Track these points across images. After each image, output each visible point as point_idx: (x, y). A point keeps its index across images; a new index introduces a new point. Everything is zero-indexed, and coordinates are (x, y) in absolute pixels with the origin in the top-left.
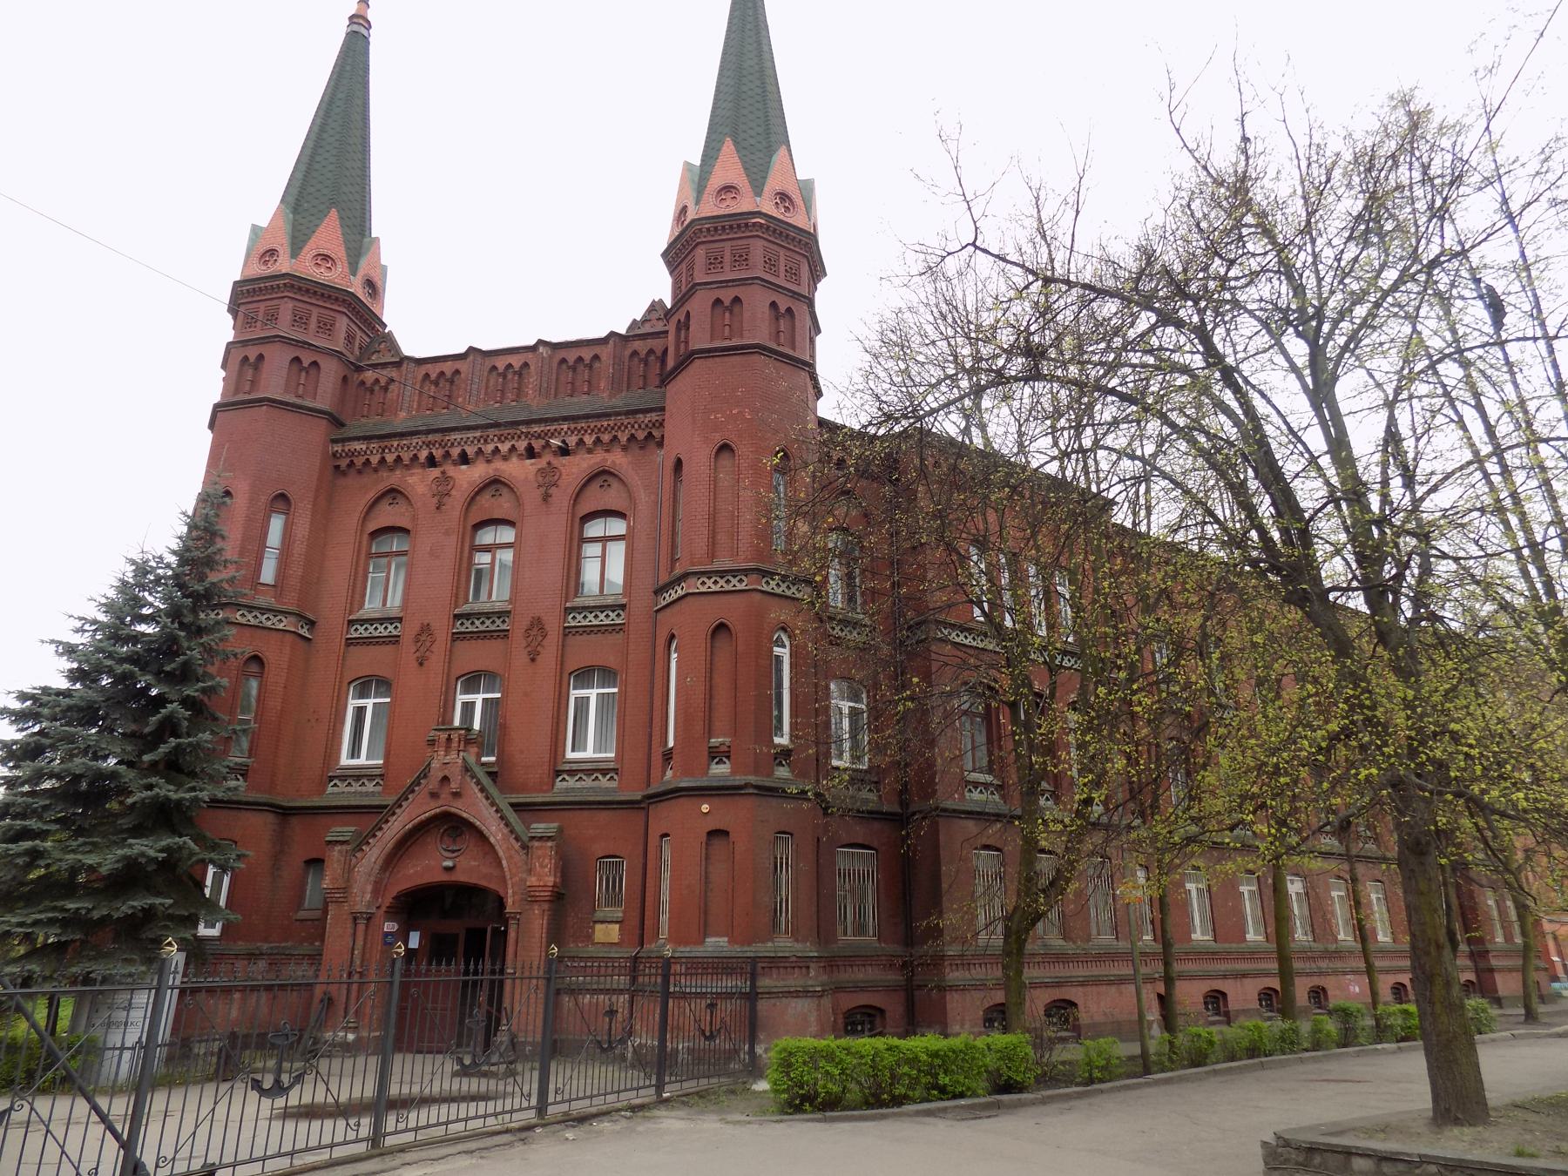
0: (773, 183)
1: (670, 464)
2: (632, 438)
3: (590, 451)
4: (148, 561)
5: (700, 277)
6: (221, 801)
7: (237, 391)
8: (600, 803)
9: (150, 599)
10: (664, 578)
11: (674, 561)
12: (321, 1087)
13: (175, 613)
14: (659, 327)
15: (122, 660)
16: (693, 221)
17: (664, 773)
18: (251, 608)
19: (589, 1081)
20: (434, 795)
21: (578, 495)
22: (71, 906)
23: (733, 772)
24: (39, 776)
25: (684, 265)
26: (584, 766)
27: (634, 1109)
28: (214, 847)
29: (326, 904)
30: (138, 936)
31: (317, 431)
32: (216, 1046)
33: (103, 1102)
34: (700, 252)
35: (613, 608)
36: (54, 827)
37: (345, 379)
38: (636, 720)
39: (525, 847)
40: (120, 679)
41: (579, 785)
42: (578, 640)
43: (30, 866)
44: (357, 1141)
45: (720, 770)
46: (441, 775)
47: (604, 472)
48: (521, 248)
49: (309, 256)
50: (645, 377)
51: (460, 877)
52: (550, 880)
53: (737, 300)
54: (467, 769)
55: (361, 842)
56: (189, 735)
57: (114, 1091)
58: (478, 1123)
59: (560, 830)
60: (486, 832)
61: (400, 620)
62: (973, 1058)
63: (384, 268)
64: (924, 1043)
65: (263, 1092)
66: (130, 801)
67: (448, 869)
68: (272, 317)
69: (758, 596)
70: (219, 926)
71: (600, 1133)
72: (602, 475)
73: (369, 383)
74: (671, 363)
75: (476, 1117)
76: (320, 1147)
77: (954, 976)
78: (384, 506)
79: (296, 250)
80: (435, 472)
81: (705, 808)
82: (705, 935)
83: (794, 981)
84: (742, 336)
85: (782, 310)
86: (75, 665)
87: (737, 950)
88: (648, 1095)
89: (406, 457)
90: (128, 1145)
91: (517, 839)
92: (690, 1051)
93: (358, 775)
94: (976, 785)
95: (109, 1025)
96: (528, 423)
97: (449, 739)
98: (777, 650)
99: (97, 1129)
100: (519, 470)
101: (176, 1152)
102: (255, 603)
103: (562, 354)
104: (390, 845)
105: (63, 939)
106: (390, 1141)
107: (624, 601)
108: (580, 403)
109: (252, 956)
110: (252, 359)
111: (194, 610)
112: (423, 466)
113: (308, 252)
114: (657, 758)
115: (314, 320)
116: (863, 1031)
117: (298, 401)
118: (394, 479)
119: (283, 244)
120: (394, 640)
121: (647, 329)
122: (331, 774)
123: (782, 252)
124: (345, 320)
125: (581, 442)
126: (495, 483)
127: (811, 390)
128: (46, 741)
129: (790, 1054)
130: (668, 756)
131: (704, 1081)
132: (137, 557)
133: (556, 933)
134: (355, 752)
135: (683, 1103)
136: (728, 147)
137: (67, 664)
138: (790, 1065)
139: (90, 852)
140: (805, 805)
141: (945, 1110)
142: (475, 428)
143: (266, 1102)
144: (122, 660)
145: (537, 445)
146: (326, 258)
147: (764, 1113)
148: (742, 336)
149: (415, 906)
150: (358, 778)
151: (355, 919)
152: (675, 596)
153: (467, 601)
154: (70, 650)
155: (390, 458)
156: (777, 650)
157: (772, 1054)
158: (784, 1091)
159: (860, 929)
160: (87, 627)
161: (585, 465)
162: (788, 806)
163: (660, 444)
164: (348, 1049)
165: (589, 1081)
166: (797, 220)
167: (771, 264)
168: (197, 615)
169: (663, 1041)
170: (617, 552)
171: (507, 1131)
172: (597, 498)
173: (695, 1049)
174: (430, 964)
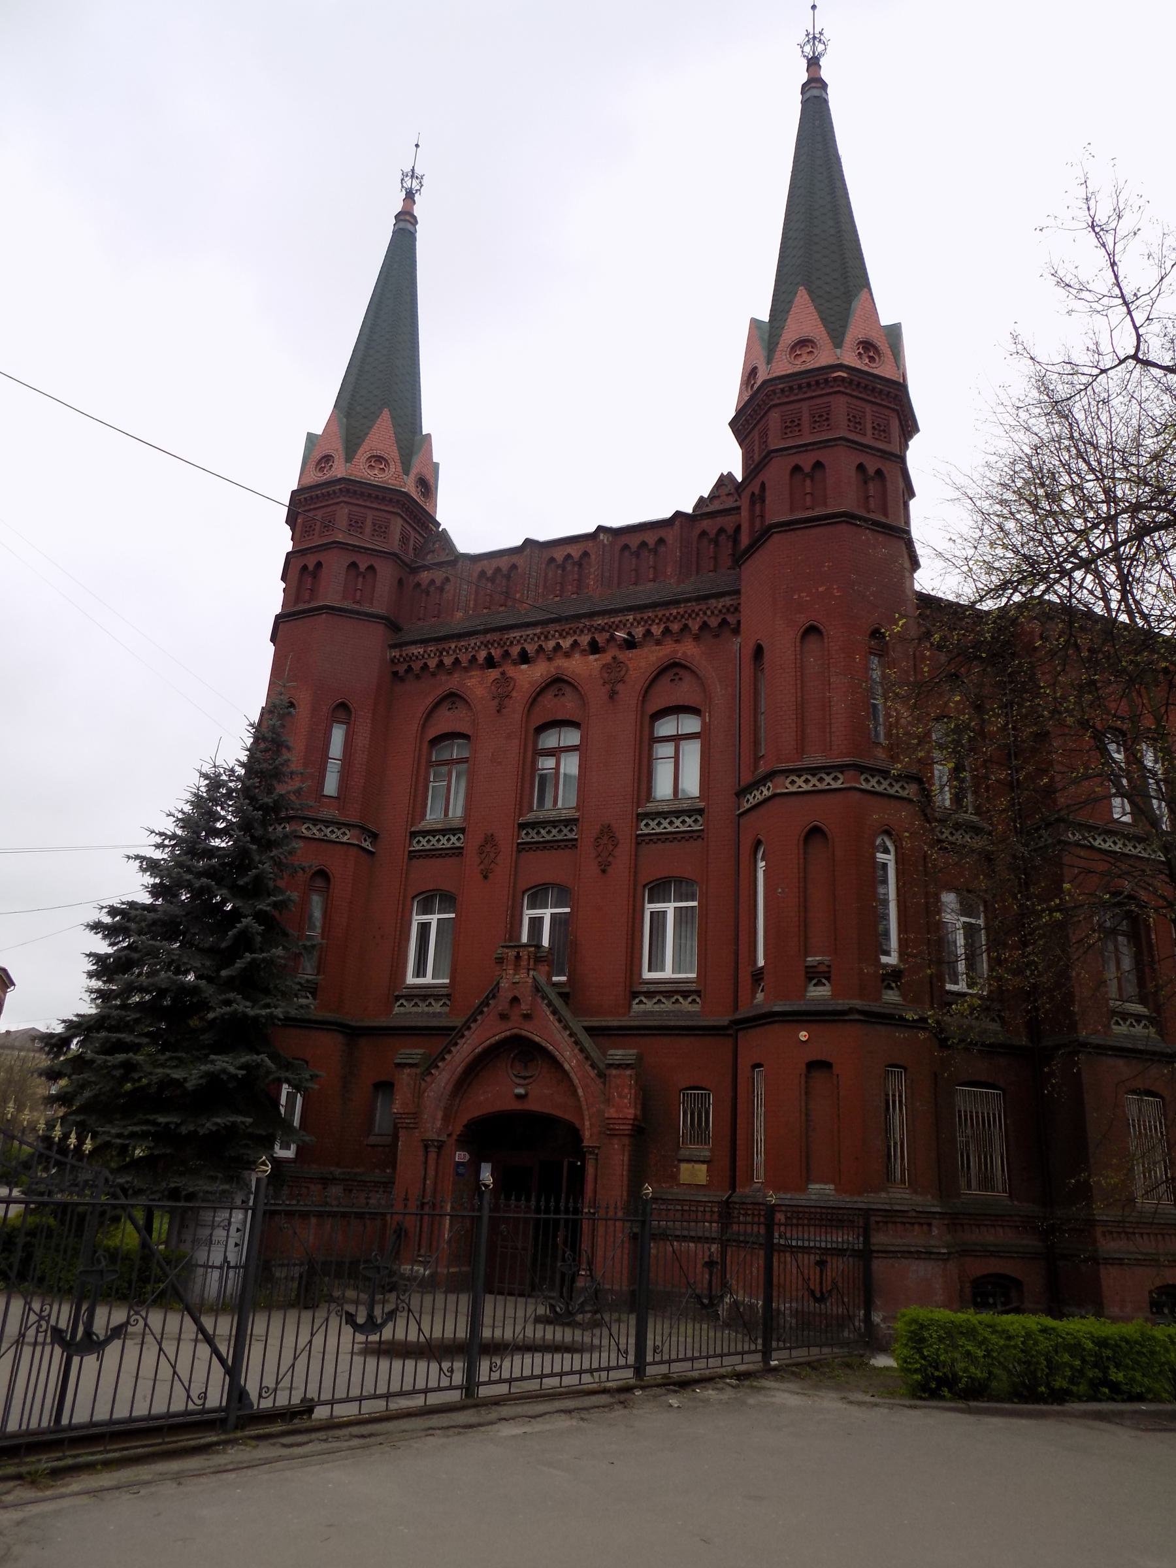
0: (855, 332)
1: (749, 651)
2: (704, 626)
4: (220, 775)
5: (775, 443)
6: (295, 1019)
7: (298, 599)
9: (223, 813)
10: (747, 778)
11: (757, 759)
12: (413, 1327)
13: (246, 825)
14: (730, 503)
15: (199, 875)
16: (765, 382)
17: (754, 997)
18: (315, 821)
19: (682, 1339)
20: (503, 1017)
21: (646, 691)
22: (162, 1120)
23: (834, 995)
24: (129, 989)
25: (756, 433)
26: (662, 988)
27: (740, 1376)
28: (288, 1066)
29: (396, 1128)
30: (225, 1157)
31: (373, 639)
32: (296, 1272)
33: (208, 1322)
34: (775, 415)
35: (689, 813)
36: (145, 1040)
37: (400, 581)
38: (719, 935)
39: (601, 1075)
40: (196, 894)
41: (657, 1008)
42: (645, 851)
43: (125, 1078)
44: (451, 1388)
45: (819, 993)
46: (510, 995)
47: (676, 665)
48: (585, 425)
49: (363, 459)
50: (715, 558)
51: (533, 1106)
52: (630, 1112)
53: (818, 465)
54: (537, 989)
55: (431, 1064)
56: (262, 951)
57: (218, 1309)
58: (554, 1382)
59: (640, 1057)
60: (559, 1057)
61: (463, 830)
62: (1153, 1353)
63: (437, 465)
64: (1080, 1327)
65: (357, 1328)
66: (211, 1016)
67: (519, 1097)
68: (328, 525)
69: (858, 795)
70: (293, 1147)
71: (706, 1401)
72: (673, 668)
73: (425, 583)
74: (745, 541)
75: (572, 1373)
76: (414, 1392)
77: (1109, 1246)
78: (444, 712)
79: (350, 454)
80: (494, 674)
81: (803, 1036)
82: (808, 1180)
83: (915, 1239)
84: (825, 504)
86: (158, 881)
87: (848, 1200)
88: (752, 1362)
89: (464, 659)
90: (233, 1371)
91: (593, 1066)
92: (796, 1314)
93: (424, 994)
94: (1125, 1016)
95: (195, 1241)
96: (592, 615)
97: (518, 957)
98: (881, 857)
99: (204, 1350)
100: (582, 666)
101: (277, 1383)
102: (320, 816)
103: (624, 540)
104: (460, 1069)
105: (156, 1152)
106: (483, 1391)
107: (702, 805)
108: (646, 592)
109: (326, 1181)
110: (311, 568)
111: (264, 823)
112: (482, 667)
114: (745, 978)
115: (369, 522)
116: (995, 1305)
117: (356, 607)
118: (453, 682)
119: (337, 448)
120: (457, 852)
121: (716, 506)
122: (399, 993)
123: (868, 408)
124: (400, 521)
125: (648, 633)
126: (557, 682)
127: (907, 564)
128: (135, 956)
129: (922, 1326)
130: (758, 976)
131: (815, 1350)
132: (207, 769)
133: (637, 1175)
134: (420, 971)
135: (793, 1373)
136: (802, 297)
137: (148, 879)
138: (923, 1340)
139: (176, 1067)
140: (922, 1035)
141: (1121, 1414)
143: (360, 1338)
144: (199, 875)
145: (601, 639)
146: (379, 459)
147: (892, 1394)
148: (825, 504)
149: (487, 1135)
150: (424, 998)
151: (426, 1147)
152: (760, 798)
153: (531, 810)
154: (151, 866)
155: (448, 661)
156: (881, 857)
157: (899, 1325)
158: (916, 1371)
159: (986, 1182)
160: (166, 842)
161: (653, 658)
162: (901, 1034)
163: (736, 631)
164: (429, 1285)
165: (682, 1339)
166: (884, 370)
167: (856, 422)
168: (266, 830)
169: (768, 1300)
170: (692, 754)
171: (605, 1391)
172: (664, 696)
173: (800, 1311)
174: (508, 1198)
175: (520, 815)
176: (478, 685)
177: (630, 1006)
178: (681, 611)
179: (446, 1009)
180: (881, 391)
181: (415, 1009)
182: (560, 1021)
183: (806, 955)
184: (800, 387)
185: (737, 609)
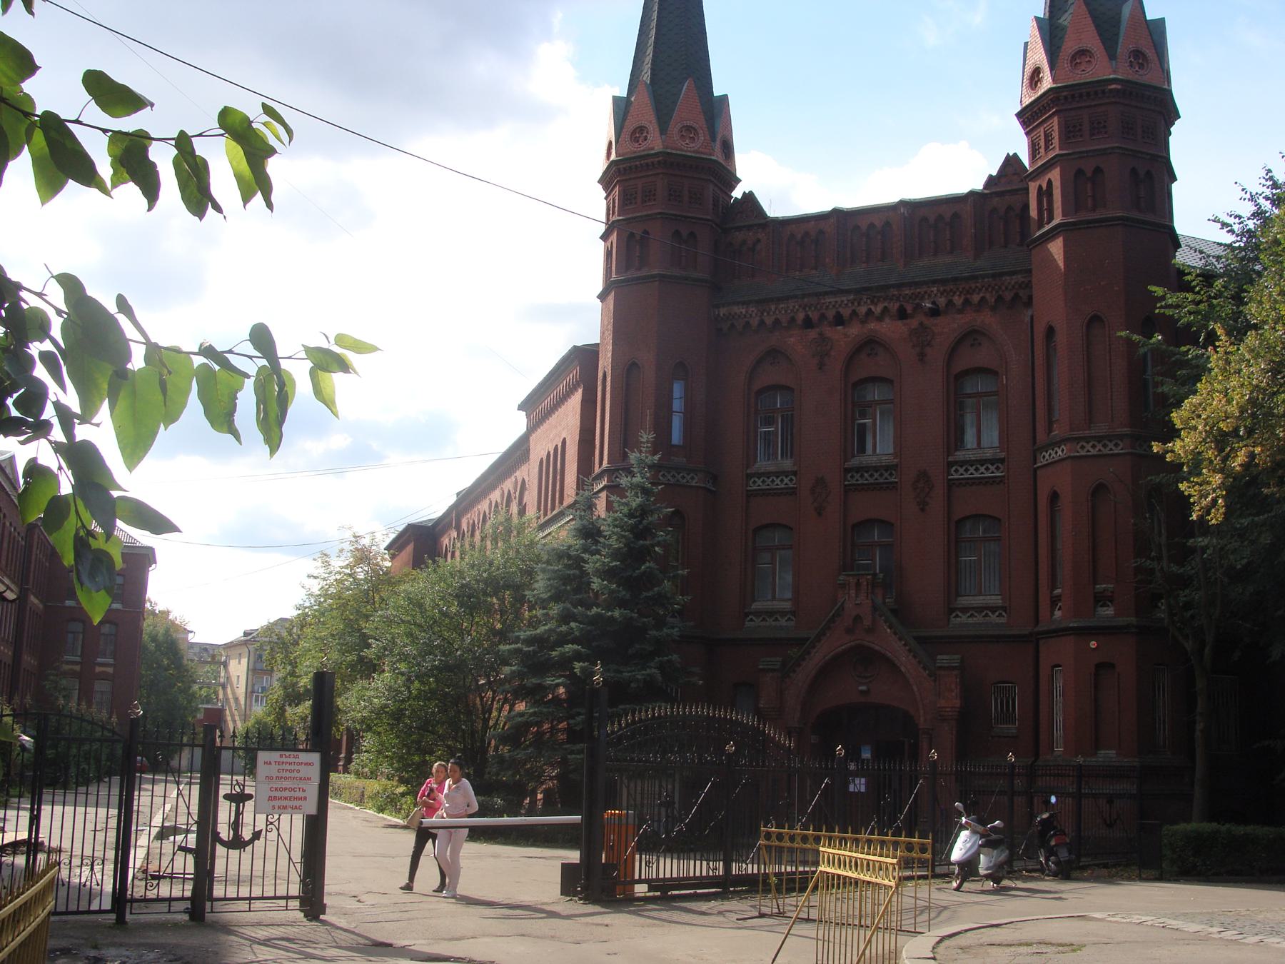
3: (960, 311)
8: (1014, 636)
17: (1052, 614)
35: (992, 462)
41: (971, 621)
53: (1098, 170)
67: (862, 692)
80: (813, 334)
81: (1093, 644)
91: (924, 668)
96: (899, 286)
100: (889, 329)
107: (1003, 455)
113: (674, 128)
119: (648, 118)
120: (792, 492)
124: (711, 187)
125: (950, 303)
126: (870, 344)
142: (848, 292)
146: (689, 129)
163: (1029, 303)
166: (1146, 77)
176: (795, 342)
177: (949, 620)
179: (793, 623)
182: (895, 633)
183: (1095, 583)
184: (1081, 96)
185: (1028, 285)
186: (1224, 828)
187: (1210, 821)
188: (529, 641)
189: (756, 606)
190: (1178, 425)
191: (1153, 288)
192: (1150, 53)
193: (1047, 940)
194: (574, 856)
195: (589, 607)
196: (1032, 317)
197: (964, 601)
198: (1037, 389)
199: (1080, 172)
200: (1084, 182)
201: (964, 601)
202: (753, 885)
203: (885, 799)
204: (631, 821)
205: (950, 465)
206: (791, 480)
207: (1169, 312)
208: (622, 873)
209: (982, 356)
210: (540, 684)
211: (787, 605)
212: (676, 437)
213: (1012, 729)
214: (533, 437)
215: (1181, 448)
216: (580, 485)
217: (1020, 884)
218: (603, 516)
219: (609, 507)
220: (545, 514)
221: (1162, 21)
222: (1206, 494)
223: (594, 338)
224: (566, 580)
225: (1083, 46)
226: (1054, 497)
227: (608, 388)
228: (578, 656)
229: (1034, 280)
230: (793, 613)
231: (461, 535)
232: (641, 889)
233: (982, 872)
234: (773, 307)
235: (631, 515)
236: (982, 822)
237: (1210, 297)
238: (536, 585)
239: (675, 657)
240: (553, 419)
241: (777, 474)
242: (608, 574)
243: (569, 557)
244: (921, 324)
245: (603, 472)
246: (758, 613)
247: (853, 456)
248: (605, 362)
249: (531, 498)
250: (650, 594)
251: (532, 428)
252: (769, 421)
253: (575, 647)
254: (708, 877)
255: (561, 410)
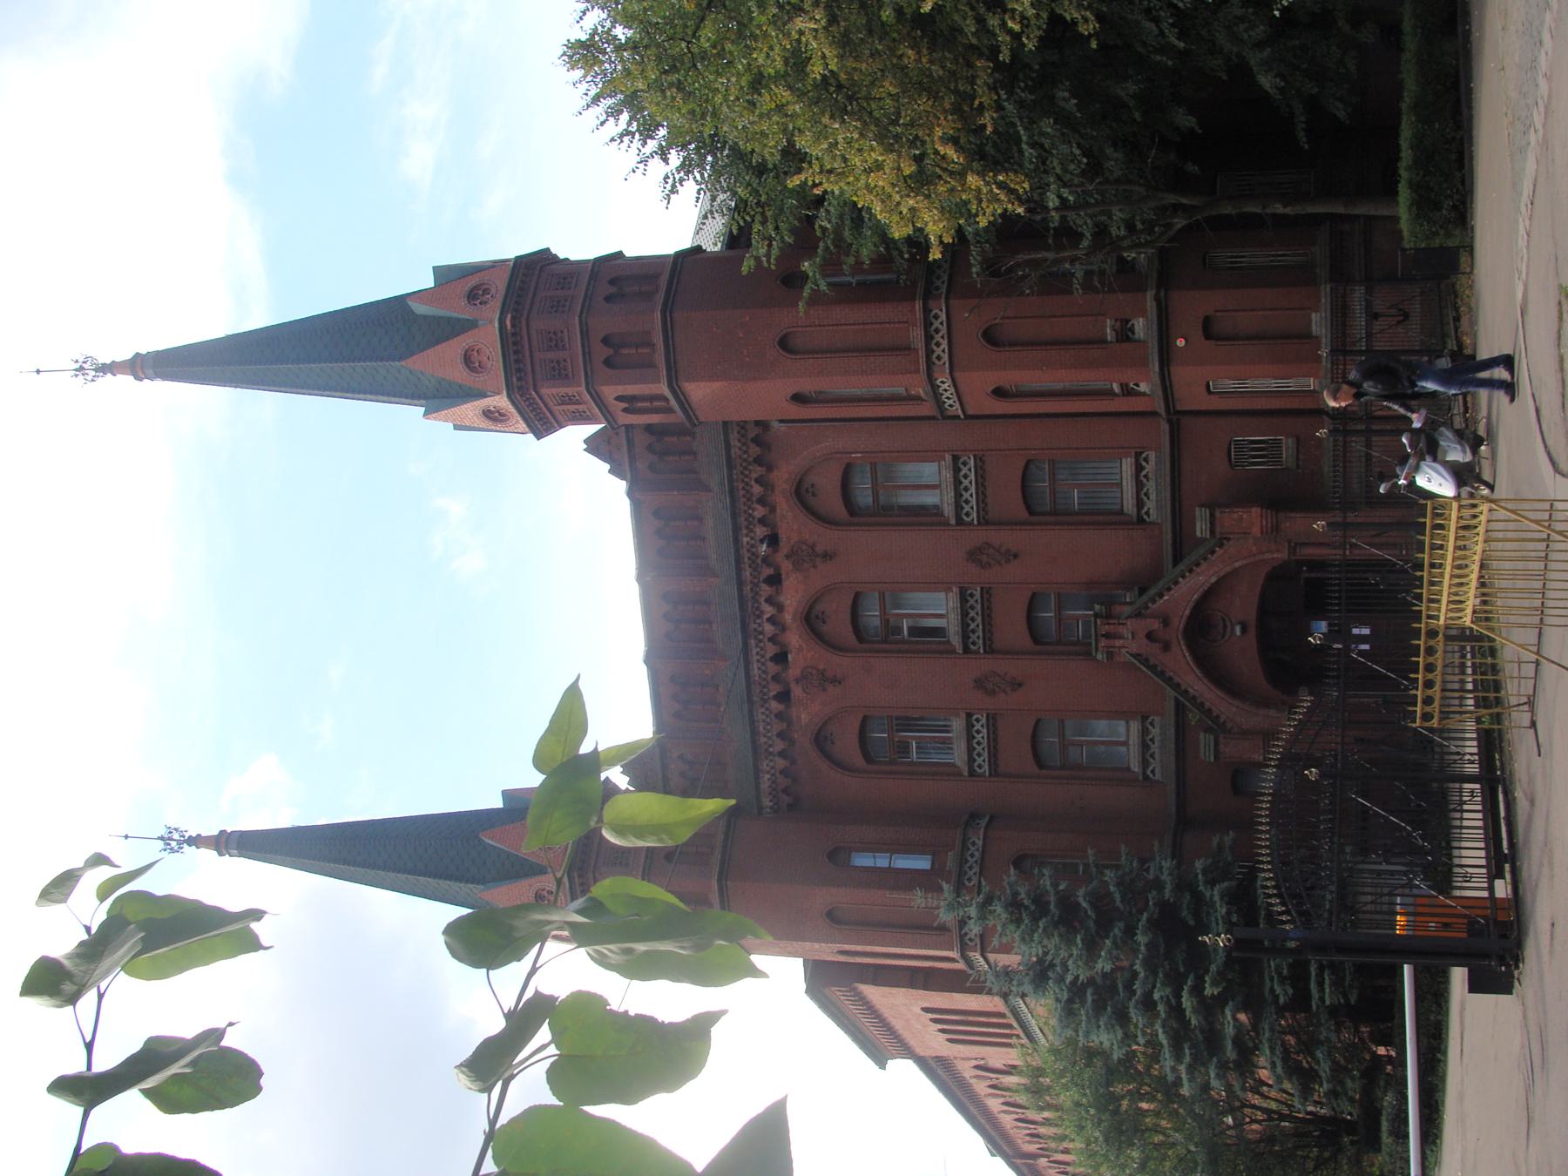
3: (773, 510)
17: (1144, 394)
20: (1166, 647)
35: (956, 470)
41: (1153, 496)
46: (1145, 641)
48: (541, 592)
51: (1252, 616)
55: (1217, 727)
67: (1244, 630)
72: (802, 494)
80: (797, 691)
81: (1181, 343)
85: (613, 290)
91: (1213, 552)
96: (741, 583)
100: (793, 597)
107: (948, 457)
120: (992, 721)
125: (762, 521)
126: (811, 621)
163: (763, 425)
166: (500, 285)
175: (954, 651)
176: (806, 713)
178: (741, 486)
180: (523, 282)
181: (1157, 756)
182: (1169, 589)
183: (1105, 342)
185: (743, 425)
186: (1404, 174)
187: (1397, 193)
188: (1178, 1057)
189: (1135, 767)
190: (909, 230)
191: (745, 270)
192: (472, 282)
193: (1543, 639)
194: (1459, 976)
195: (1135, 975)
196: (781, 421)
197: (1129, 506)
198: (868, 415)
199: (608, 363)
200: (617, 355)
201: (1129, 506)
202: (1492, 743)
203: (1377, 584)
204: (1409, 900)
205: (960, 522)
206: (978, 720)
207: (775, 252)
208: (1479, 912)
209: (827, 486)
210: (1234, 1043)
211: (1135, 726)
212: (922, 863)
213: (1287, 444)
214: (920, 1051)
215: (936, 227)
216: (978, 989)
217: (1484, 412)
218: (1019, 958)
219: (1006, 949)
220: (1018, 1036)
221: (435, 269)
222: (991, 198)
223: (798, 963)
224: (1099, 1008)
225: (460, 360)
226: (999, 393)
227: (859, 948)
228: (1197, 990)
229: (736, 418)
230: (1144, 718)
231: (1044, 1152)
232: (1502, 889)
233: (1468, 458)
234: (763, 740)
235: (1018, 922)
236: (1404, 459)
237: (758, 204)
238: (1106, 1044)
239: (1199, 865)
240: (898, 1025)
241: (970, 738)
242: (1092, 948)
243: (1070, 1001)
244: (787, 557)
245: (964, 956)
246: (1145, 763)
247: (948, 642)
248: (828, 951)
249: (998, 1057)
250: (1117, 896)
251: (907, 1051)
252: (904, 748)
253: (1185, 994)
254: (1483, 803)
255: (887, 1013)
